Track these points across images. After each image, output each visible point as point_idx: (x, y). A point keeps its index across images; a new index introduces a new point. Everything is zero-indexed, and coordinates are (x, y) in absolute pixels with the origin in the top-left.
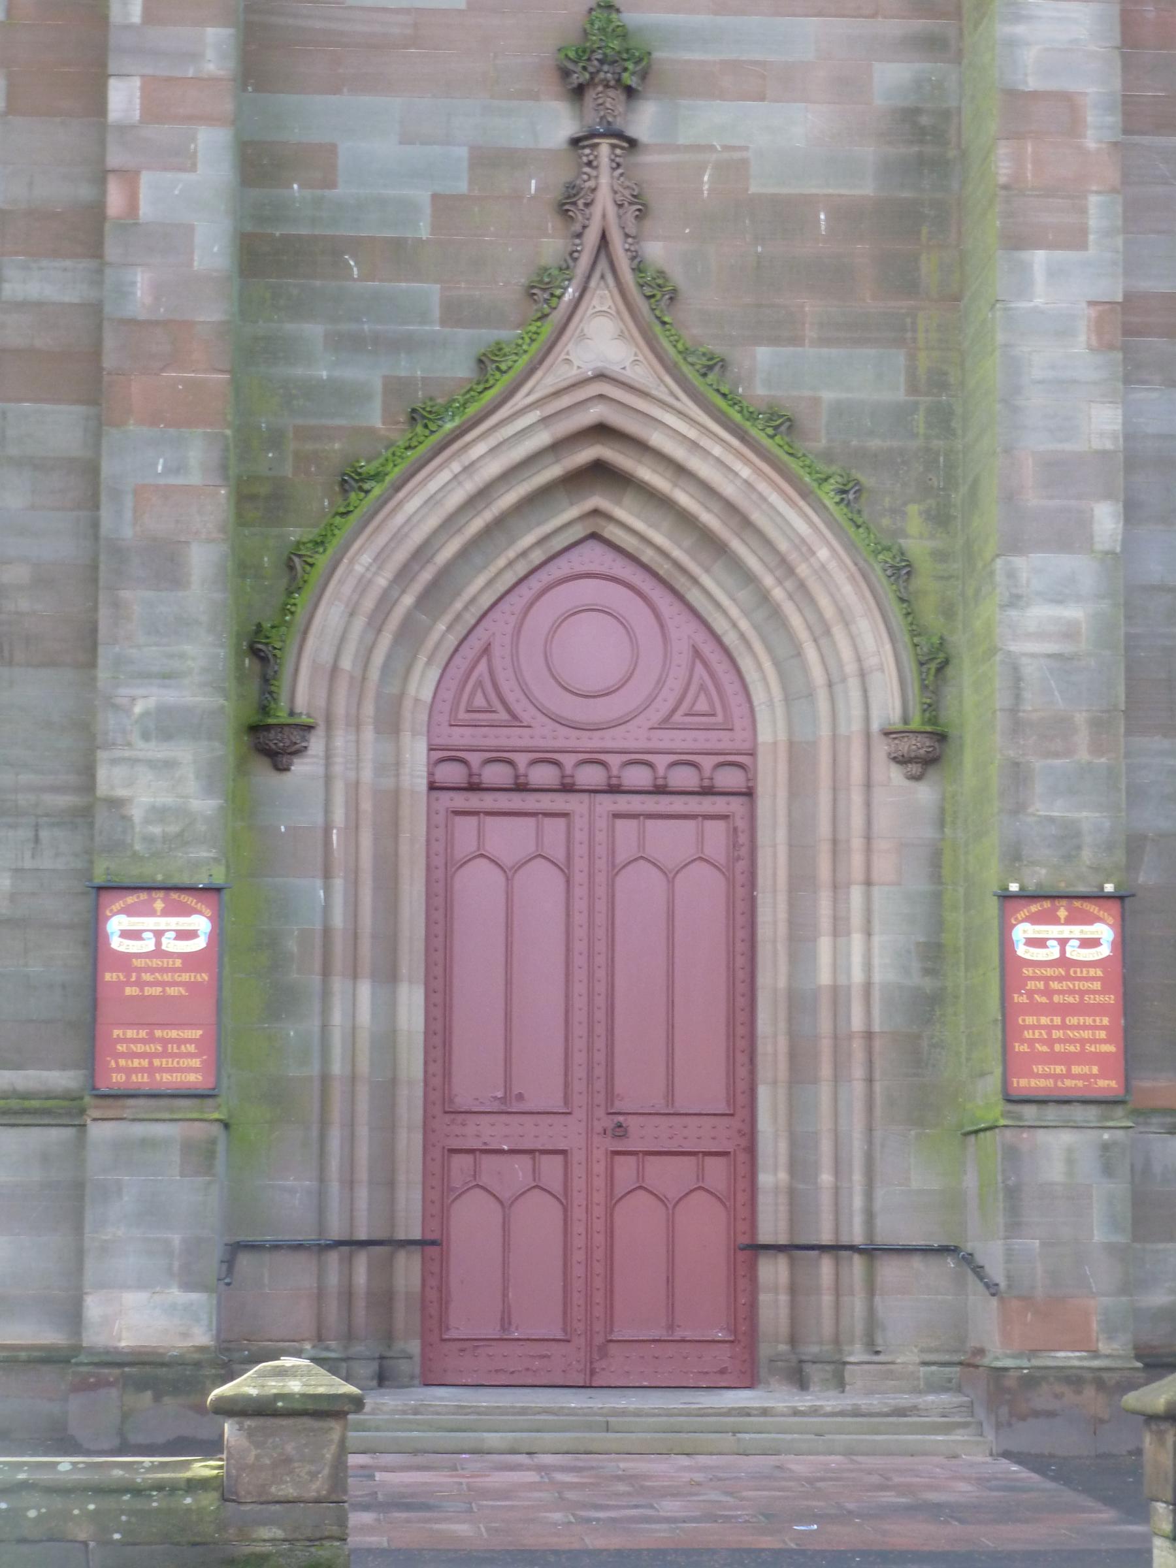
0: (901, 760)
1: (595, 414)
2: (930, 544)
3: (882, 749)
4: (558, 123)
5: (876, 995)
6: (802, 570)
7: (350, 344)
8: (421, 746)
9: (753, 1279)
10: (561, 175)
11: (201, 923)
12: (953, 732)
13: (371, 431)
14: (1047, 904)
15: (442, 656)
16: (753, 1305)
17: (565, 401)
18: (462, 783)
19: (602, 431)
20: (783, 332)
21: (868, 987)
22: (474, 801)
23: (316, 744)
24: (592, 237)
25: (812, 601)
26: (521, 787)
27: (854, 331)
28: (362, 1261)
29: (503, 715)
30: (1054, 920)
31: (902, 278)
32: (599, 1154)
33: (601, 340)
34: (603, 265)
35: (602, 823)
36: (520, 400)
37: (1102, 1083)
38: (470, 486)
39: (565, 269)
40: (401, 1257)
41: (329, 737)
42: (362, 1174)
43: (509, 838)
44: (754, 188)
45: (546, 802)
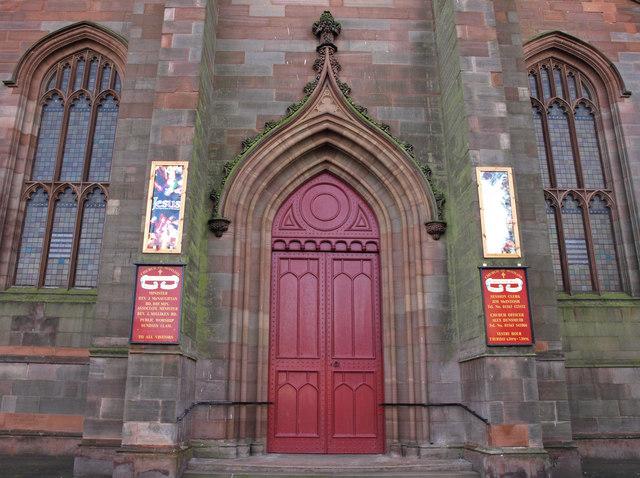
0: (431, 233)
1: (325, 125)
2: (435, 166)
3: (424, 231)
4: (313, 45)
5: (427, 313)
6: (395, 172)
7: (249, 106)
8: (269, 235)
9: (384, 419)
10: (315, 57)
11: (175, 278)
12: (448, 224)
13: (252, 131)
14: (498, 271)
15: (276, 206)
16: (384, 425)
17: (316, 121)
18: (285, 248)
19: (327, 132)
20: (382, 101)
21: (424, 311)
22: (287, 255)
23: (231, 228)
24: (323, 74)
25: (399, 183)
26: (302, 250)
27: (408, 103)
28: (244, 410)
29: (297, 227)
30: (500, 277)
31: (423, 89)
32: (329, 373)
33: (327, 104)
34: (327, 82)
35: (329, 262)
36: (301, 120)
37: (523, 339)
38: (284, 147)
39: (315, 83)
40: (259, 408)
41: (235, 226)
42: (244, 378)
43: (300, 267)
44: (374, 63)
45: (311, 255)
